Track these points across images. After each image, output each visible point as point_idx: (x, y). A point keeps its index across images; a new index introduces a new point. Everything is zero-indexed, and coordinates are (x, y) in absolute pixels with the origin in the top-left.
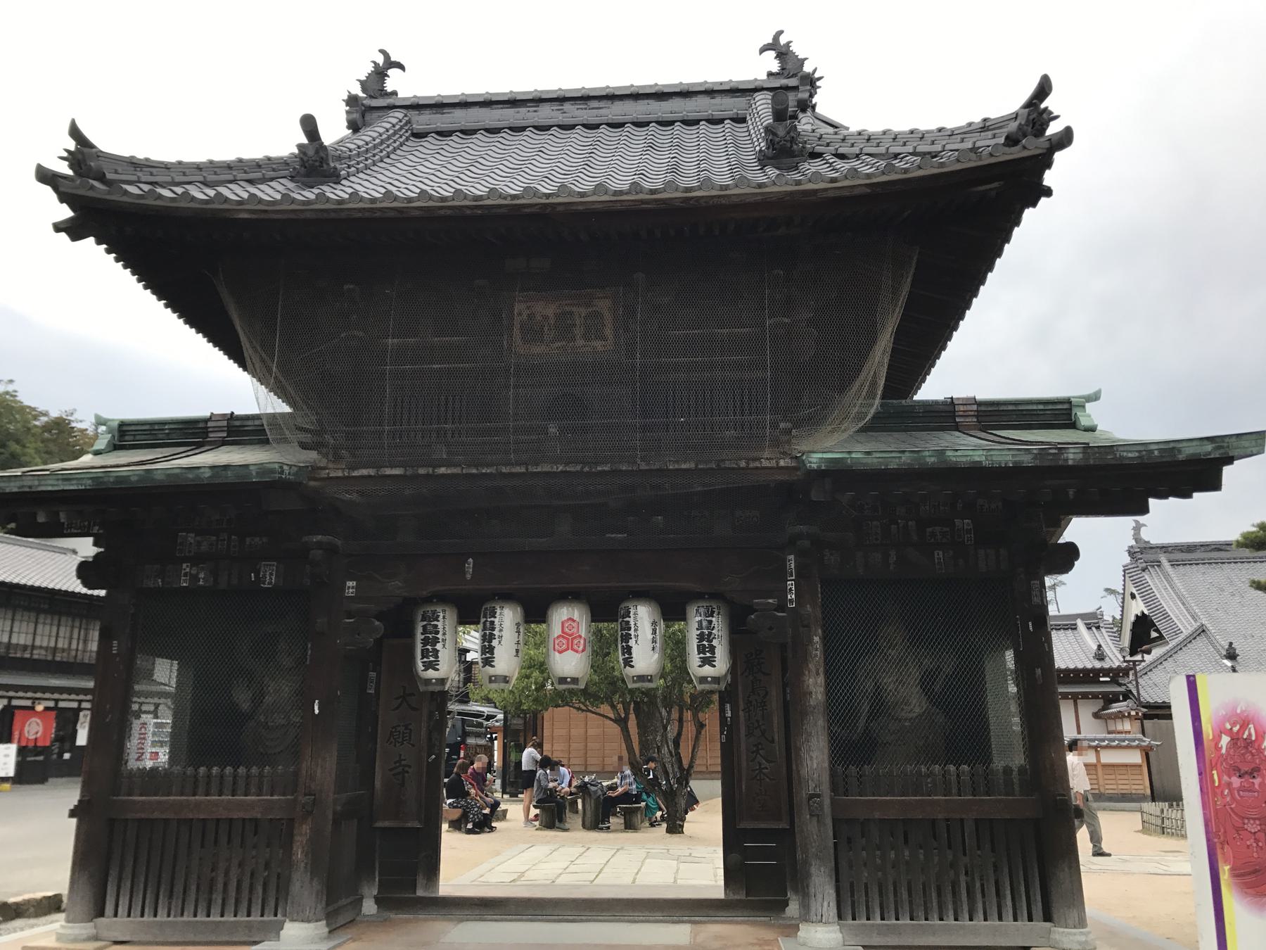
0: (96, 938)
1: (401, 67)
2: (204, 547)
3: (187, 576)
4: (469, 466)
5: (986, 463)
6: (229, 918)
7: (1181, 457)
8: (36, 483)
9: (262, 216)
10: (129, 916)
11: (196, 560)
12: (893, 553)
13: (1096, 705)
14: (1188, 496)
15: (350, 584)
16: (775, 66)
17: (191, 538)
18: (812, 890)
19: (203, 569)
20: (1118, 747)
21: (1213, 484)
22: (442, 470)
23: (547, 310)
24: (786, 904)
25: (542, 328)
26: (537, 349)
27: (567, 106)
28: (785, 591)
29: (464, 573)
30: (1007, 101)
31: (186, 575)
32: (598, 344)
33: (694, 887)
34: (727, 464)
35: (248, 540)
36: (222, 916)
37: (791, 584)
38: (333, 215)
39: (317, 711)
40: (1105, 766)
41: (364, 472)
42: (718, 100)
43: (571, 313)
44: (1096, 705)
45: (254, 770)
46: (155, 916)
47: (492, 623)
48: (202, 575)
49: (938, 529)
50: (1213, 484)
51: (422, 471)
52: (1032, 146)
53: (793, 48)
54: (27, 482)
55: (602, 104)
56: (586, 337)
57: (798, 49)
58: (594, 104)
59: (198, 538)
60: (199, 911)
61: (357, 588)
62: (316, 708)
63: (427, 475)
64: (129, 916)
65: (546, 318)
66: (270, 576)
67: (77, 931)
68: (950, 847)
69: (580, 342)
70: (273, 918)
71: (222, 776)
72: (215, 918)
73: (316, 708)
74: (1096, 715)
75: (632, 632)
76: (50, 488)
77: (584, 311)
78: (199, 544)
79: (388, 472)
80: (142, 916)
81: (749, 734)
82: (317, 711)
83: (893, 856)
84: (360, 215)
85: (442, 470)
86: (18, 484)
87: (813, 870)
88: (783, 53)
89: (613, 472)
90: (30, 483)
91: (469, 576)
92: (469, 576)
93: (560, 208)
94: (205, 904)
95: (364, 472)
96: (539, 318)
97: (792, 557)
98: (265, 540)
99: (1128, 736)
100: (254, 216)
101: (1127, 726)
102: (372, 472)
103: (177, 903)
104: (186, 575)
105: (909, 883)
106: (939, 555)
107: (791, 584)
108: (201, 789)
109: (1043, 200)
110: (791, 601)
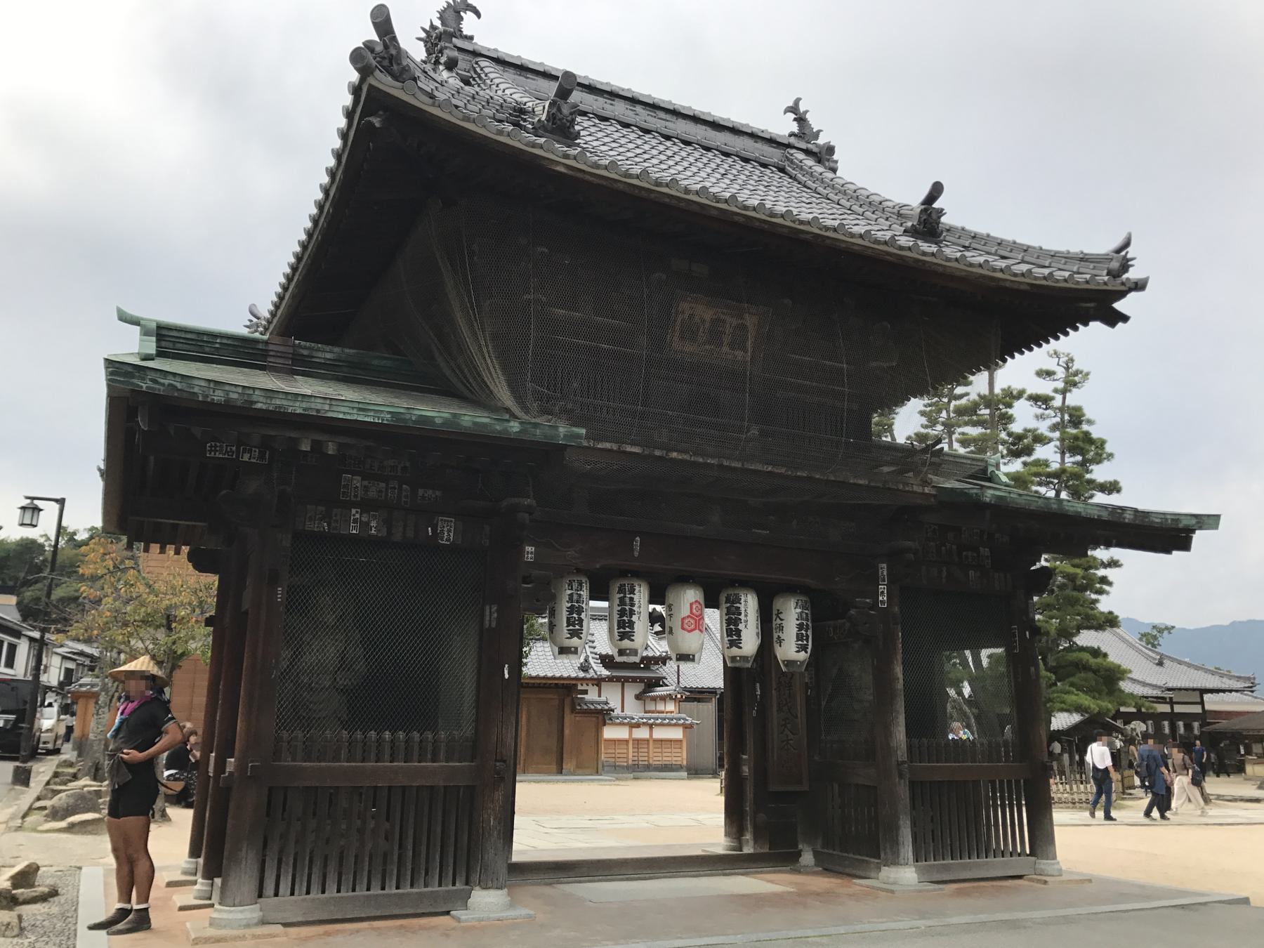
0: (263, 922)
1: (478, 14)
2: (372, 494)
3: (355, 523)
4: (695, 454)
5: (1083, 514)
6: (406, 890)
7: (1181, 526)
8: (327, 407)
9: (579, 175)
10: (292, 894)
11: (366, 506)
12: (944, 569)
13: (637, 689)
14: (1168, 551)
15: (529, 549)
16: (795, 128)
17: (357, 481)
18: (901, 839)
19: (375, 517)
20: (669, 725)
21: (1185, 545)
22: (674, 455)
23: (705, 313)
24: (799, 854)
25: (698, 329)
26: (689, 348)
27: (639, 108)
28: (876, 594)
29: (632, 550)
30: (1102, 245)
31: (355, 521)
32: (739, 354)
33: (570, 850)
34: (891, 485)
35: (421, 492)
36: (368, 889)
37: (882, 588)
38: (644, 194)
39: (507, 676)
40: (655, 741)
41: (608, 445)
42: (759, 145)
43: (724, 321)
44: (639, 688)
45: (401, 735)
46: (323, 892)
47: (631, 599)
48: (373, 524)
49: (970, 553)
50: (1185, 545)
51: (657, 453)
52: (1115, 286)
53: (808, 116)
54: (317, 404)
55: (668, 117)
56: (732, 346)
57: (814, 122)
58: (662, 114)
59: (366, 483)
60: (373, 883)
61: (536, 553)
62: (506, 672)
63: (660, 457)
64: (292, 894)
65: (703, 321)
66: (448, 533)
67: (248, 915)
68: (388, 820)
69: (725, 349)
70: (451, 887)
71: (380, 741)
72: (376, 891)
73: (506, 672)
74: (638, 697)
75: (742, 617)
76: (341, 416)
77: (735, 322)
78: (366, 489)
79: (629, 449)
80: (308, 893)
81: (780, 710)
82: (507, 676)
83: (344, 827)
84: (667, 200)
85: (674, 455)
86: (304, 405)
87: (901, 822)
88: (801, 120)
89: (809, 479)
90: (319, 407)
91: (636, 554)
92: (636, 554)
93: (828, 241)
94: (379, 876)
95: (608, 445)
96: (697, 319)
97: (884, 565)
98: (438, 493)
99: (669, 715)
100: (570, 173)
101: (671, 707)
102: (615, 447)
103: (348, 879)
104: (355, 521)
105: (296, 854)
106: (971, 573)
107: (882, 588)
108: (416, 756)
109: (1120, 325)
110: (882, 602)
